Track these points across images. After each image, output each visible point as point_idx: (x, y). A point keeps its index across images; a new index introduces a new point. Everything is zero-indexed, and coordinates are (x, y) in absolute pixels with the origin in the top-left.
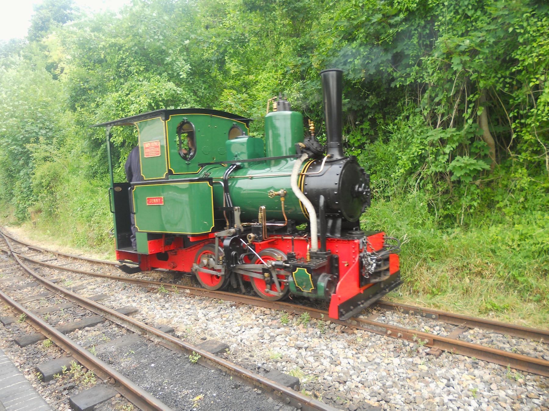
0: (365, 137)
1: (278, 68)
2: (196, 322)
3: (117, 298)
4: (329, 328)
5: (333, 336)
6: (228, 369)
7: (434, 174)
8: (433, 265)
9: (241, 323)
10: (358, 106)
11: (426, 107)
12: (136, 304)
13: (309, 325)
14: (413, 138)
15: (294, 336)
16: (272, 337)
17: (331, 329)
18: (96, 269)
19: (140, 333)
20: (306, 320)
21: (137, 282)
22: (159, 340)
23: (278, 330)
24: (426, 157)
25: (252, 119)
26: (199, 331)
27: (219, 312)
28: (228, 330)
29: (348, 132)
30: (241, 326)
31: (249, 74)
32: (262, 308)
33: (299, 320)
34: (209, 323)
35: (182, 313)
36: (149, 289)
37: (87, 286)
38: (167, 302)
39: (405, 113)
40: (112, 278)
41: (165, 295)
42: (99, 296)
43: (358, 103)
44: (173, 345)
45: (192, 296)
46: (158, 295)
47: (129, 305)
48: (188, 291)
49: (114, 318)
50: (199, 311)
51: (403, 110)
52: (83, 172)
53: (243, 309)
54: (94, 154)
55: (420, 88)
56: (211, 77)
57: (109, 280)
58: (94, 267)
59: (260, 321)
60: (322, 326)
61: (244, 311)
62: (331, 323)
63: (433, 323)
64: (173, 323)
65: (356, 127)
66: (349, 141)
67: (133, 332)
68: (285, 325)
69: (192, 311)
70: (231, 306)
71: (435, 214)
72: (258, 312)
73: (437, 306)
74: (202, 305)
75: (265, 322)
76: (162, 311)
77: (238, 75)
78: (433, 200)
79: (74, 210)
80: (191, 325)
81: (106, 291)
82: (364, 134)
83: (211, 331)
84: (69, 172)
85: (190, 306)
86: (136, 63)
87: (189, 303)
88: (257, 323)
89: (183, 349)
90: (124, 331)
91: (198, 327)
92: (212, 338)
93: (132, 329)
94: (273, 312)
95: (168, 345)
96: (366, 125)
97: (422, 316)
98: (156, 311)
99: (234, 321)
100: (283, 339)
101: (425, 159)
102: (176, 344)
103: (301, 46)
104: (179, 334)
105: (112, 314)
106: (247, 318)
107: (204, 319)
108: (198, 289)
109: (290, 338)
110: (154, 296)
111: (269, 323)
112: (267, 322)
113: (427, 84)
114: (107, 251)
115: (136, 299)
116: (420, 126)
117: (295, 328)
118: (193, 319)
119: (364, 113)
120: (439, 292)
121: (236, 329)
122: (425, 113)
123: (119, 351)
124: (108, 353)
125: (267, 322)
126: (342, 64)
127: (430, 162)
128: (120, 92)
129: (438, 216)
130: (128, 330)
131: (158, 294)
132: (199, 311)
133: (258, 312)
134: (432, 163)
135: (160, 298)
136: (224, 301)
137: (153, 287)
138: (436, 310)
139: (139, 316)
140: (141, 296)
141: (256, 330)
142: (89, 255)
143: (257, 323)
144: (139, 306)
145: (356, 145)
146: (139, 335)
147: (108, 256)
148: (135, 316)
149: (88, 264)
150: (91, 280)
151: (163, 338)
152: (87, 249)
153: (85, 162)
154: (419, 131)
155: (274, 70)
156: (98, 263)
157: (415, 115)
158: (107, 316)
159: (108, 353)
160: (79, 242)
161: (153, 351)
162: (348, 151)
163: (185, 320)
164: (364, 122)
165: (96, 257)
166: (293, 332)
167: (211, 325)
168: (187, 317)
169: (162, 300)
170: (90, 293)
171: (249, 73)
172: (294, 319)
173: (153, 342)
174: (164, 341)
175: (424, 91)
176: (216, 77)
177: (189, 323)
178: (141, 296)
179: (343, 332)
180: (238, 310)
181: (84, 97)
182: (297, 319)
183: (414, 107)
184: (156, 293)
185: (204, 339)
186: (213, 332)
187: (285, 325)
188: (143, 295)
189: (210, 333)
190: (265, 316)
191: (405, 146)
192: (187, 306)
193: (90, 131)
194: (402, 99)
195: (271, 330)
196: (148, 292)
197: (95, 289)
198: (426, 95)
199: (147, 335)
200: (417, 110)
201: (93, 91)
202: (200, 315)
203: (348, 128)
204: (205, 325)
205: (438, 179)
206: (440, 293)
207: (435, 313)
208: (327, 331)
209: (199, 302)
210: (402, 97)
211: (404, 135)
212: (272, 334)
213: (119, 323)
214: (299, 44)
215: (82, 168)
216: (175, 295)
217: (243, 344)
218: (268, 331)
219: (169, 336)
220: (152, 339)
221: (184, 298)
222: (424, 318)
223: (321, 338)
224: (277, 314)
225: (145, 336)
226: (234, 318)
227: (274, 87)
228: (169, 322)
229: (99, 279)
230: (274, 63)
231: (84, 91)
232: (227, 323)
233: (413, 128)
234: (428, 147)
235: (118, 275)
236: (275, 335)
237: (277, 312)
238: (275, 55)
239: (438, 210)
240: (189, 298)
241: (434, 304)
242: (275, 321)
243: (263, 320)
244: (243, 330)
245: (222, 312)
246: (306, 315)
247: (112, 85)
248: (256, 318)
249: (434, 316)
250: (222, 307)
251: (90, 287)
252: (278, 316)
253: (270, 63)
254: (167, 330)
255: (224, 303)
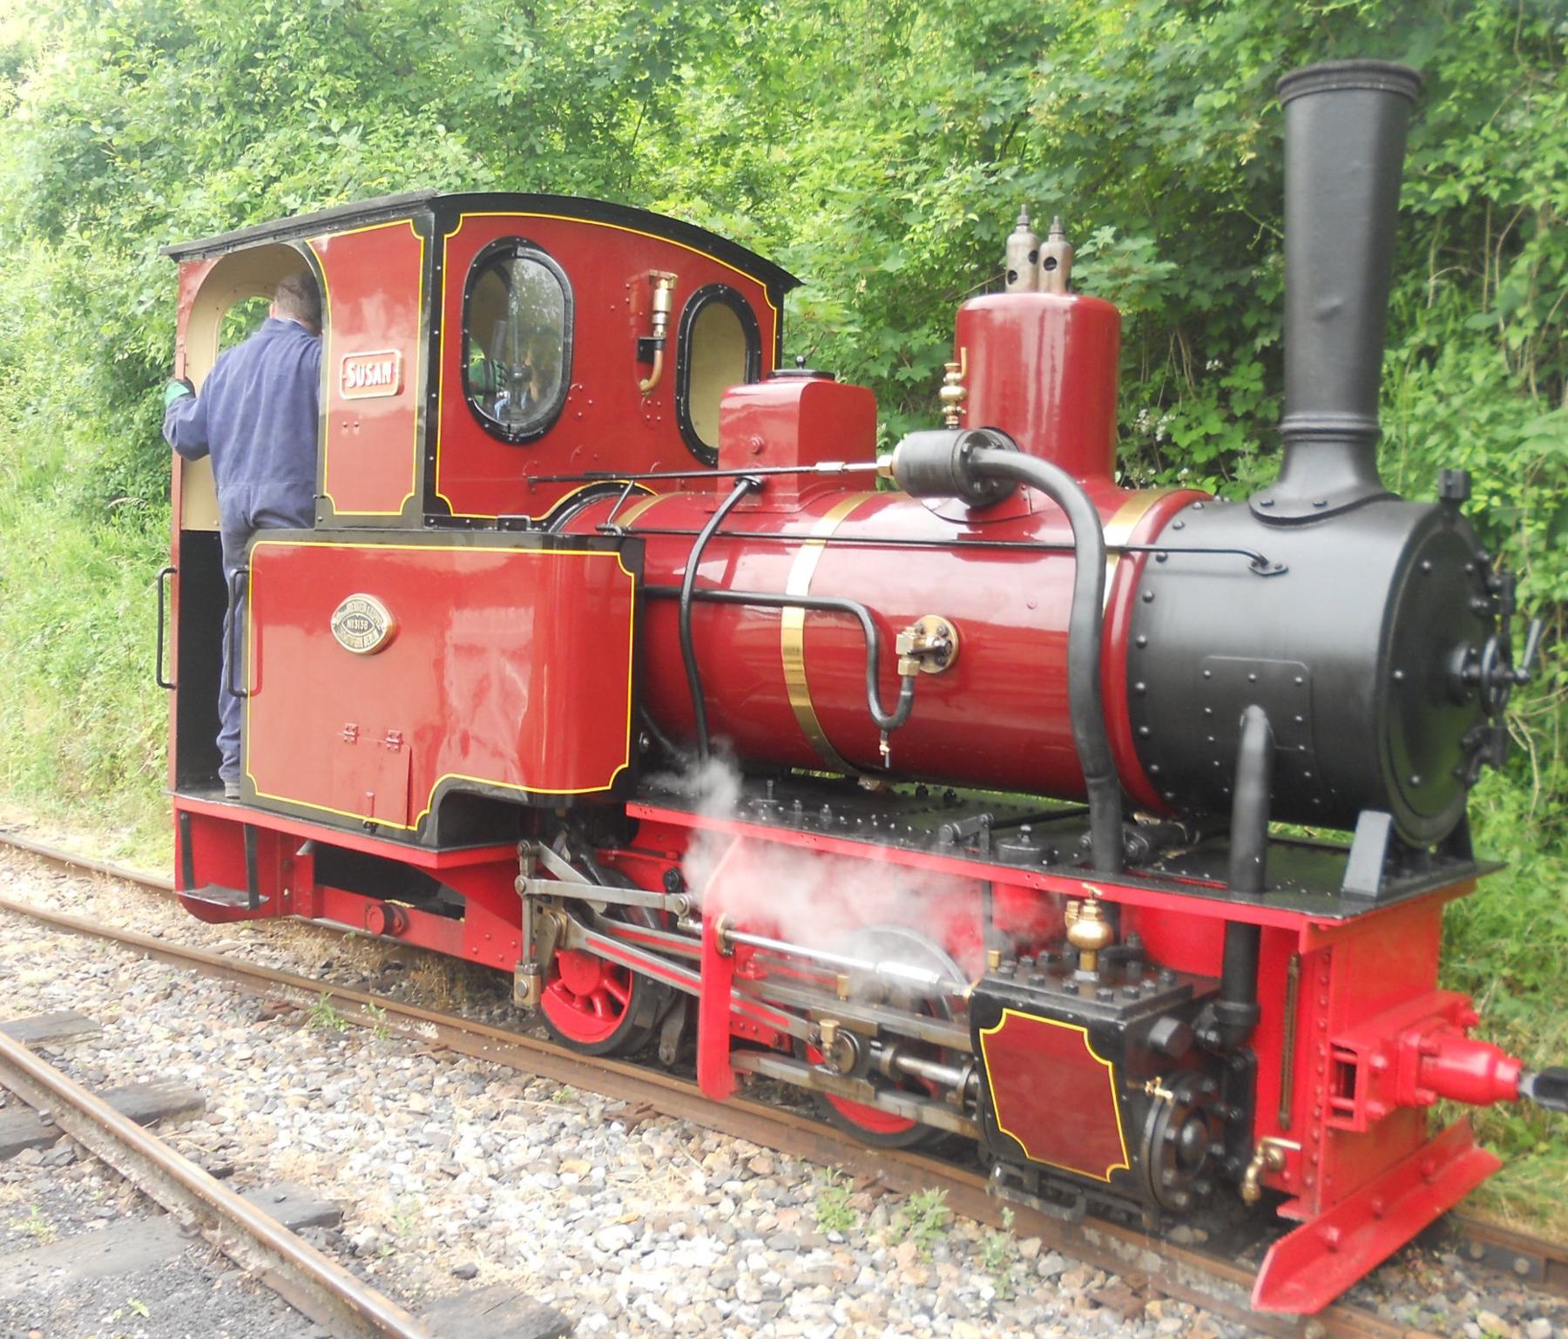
0: (1239, 426)
1: (889, 116)
2: (446, 1182)
3: (130, 1037)
4: (1034, 1273)
5: (1047, 1320)
6: (720, 1105)
7: (1540, 610)
8: (1515, 1014)
9: (638, 1207)
10: (1216, 293)
11: (1521, 312)
12: (202, 1069)
13: (941, 1251)
14: (1451, 447)
15: (868, 1298)
16: (773, 1293)
17: (1040, 1278)
18: (70, 895)
19: (189, 1218)
20: (929, 1222)
21: (223, 969)
22: (266, 1264)
23: (799, 1259)
24: (1508, 532)
25: (1086, 616)
26: (452, 1228)
27: (550, 1141)
28: (578, 1239)
29: (1165, 401)
30: (638, 1224)
31: (771, 141)
32: (739, 1145)
33: (898, 1219)
34: (502, 1191)
35: (391, 1134)
36: (267, 1007)
37: (19, 968)
38: (337, 1072)
39: (1421, 336)
40: (126, 943)
41: (329, 1039)
42: (60, 1019)
43: (1219, 282)
44: (321, 1297)
45: (445, 1053)
46: (304, 1038)
47: (173, 1070)
48: (429, 1032)
49: (94, 1133)
50: (463, 1128)
51: (1412, 321)
52: (67, 492)
53: (658, 1140)
54: (119, 417)
55: (1497, 228)
56: (613, 142)
57: (112, 950)
58: (63, 889)
59: (727, 1206)
60: (1000, 1267)
61: (658, 1152)
62: (1046, 1250)
63: (1519, 1300)
64: (344, 1174)
65: (1199, 383)
66: (1168, 437)
67: (164, 1211)
68: (835, 1236)
69: (433, 1127)
70: (608, 1122)
71: (1530, 782)
72: (719, 1160)
73: (1531, 1213)
74: (483, 1103)
75: (746, 1214)
76: (305, 1116)
77: (724, 140)
78: (1526, 721)
79: (19, 643)
80: (422, 1199)
81: (91, 999)
82: (1238, 412)
83: (503, 1234)
84: (20, 488)
85: (431, 1100)
86: (321, 62)
87: (425, 1091)
88: (709, 1214)
89: (358, 1320)
90: (125, 1199)
91: (447, 1209)
92: (503, 1274)
93: (162, 1195)
94: (787, 1164)
95: (301, 1291)
96: (1248, 378)
97: (1465, 1254)
98: (280, 1111)
99: (608, 1193)
100: (819, 1311)
101: (1500, 541)
102: (333, 1292)
103: (995, 30)
104: (360, 1235)
105: (85, 1114)
106: (670, 1187)
107: (479, 1169)
108: (475, 1027)
109: (854, 1304)
110: (285, 1038)
111: (765, 1221)
112: (756, 1214)
113: (1529, 212)
114: (131, 820)
115: (206, 1044)
116: (1487, 396)
117: (879, 1255)
118: (432, 1167)
119: (1241, 327)
120: (1538, 1138)
121: (614, 1236)
122: (1515, 337)
123: (85, 1296)
124: (33, 1304)
125: (756, 1214)
126: (1161, 108)
127: (1524, 552)
128: (240, 169)
129: (1542, 790)
130: (142, 1196)
131: (302, 1033)
132: (463, 1128)
133: (719, 1160)
134: (1533, 555)
135: (311, 1053)
136: (576, 1094)
137: (288, 997)
138: (1527, 1228)
139: (203, 1131)
140: (229, 1033)
141: (703, 1251)
142: (54, 832)
143: (709, 1214)
144: (211, 1080)
145: (1200, 457)
146: (185, 1229)
147: (128, 843)
148: (186, 1126)
149: (43, 872)
150: (39, 941)
151: (283, 1257)
152: (53, 804)
153: (83, 453)
154: (1483, 415)
155: (872, 122)
156: (82, 870)
157: (1465, 341)
158: (68, 1118)
159: (33, 1304)
160: (26, 774)
161: (232, 1313)
162: (1162, 479)
163: (397, 1168)
164: (1236, 362)
165: (80, 845)
166: (866, 1276)
167: (508, 1205)
168: (407, 1155)
169: (315, 1063)
170: (23, 1003)
171: (772, 135)
172: (879, 1214)
173: (236, 1266)
174: (285, 1272)
175: (1514, 246)
176: (632, 144)
177: (413, 1183)
178: (229, 1033)
179: (1096, 1304)
180: (633, 1143)
181: (96, 182)
182: (889, 1212)
183: (1462, 311)
184: (297, 1026)
185: (468, 1274)
186: (510, 1240)
187: (835, 1236)
188: (238, 1032)
189: (497, 1243)
190: (751, 1184)
191: (1412, 477)
192: (417, 1102)
193: (110, 329)
194: (1406, 278)
195: (771, 1255)
196: (263, 1018)
197: (45, 984)
198: (1523, 263)
199: (218, 1233)
200: (1479, 321)
201: (136, 164)
202: (466, 1152)
203: (1170, 383)
204: (481, 1203)
205: (1553, 631)
206: (1542, 1147)
207: (1529, 1245)
208: (1022, 1291)
209: (472, 1086)
210: (1406, 269)
211: (1414, 429)
212: (771, 1278)
213: (111, 1155)
214: (986, 20)
215: (69, 476)
216: (367, 1059)
217: (635, 1317)
218: (757, 1262)
219: (305, 1251)
220: (235, 1254)
221: (407, 1063)
222: (1475, 1268)
223: (991, 1318)
224: (805, 1179)
225: (207, 1233)
226: (612, 1180)
227: (870, 191)
228: (328, 1172)
229: (70, 942)
230: (875, 93)
231: (98, 159)
232: (579, 1202)
233: (1457, 402)
234: (1520, 486)
235: (156, 930)
236: (786, 1285)
237: (807, 1168)
238: (883, 62)
239: (1544, 765)
240: (432, 1067)
241: (1512, 1198)
242: (791, 1216)
243: (737, 1201)
244: (644, 1244)
245: (561, 1147)
246: (932, 1200)
247: (214, 140)
248: (709, 1187)
249: (1522, 1265)
250: (565, 1118)
251: (26, 976)
252: (808, 1190)
253: (861, 94)
254: (309, 1213)
255: (577, 1103)
